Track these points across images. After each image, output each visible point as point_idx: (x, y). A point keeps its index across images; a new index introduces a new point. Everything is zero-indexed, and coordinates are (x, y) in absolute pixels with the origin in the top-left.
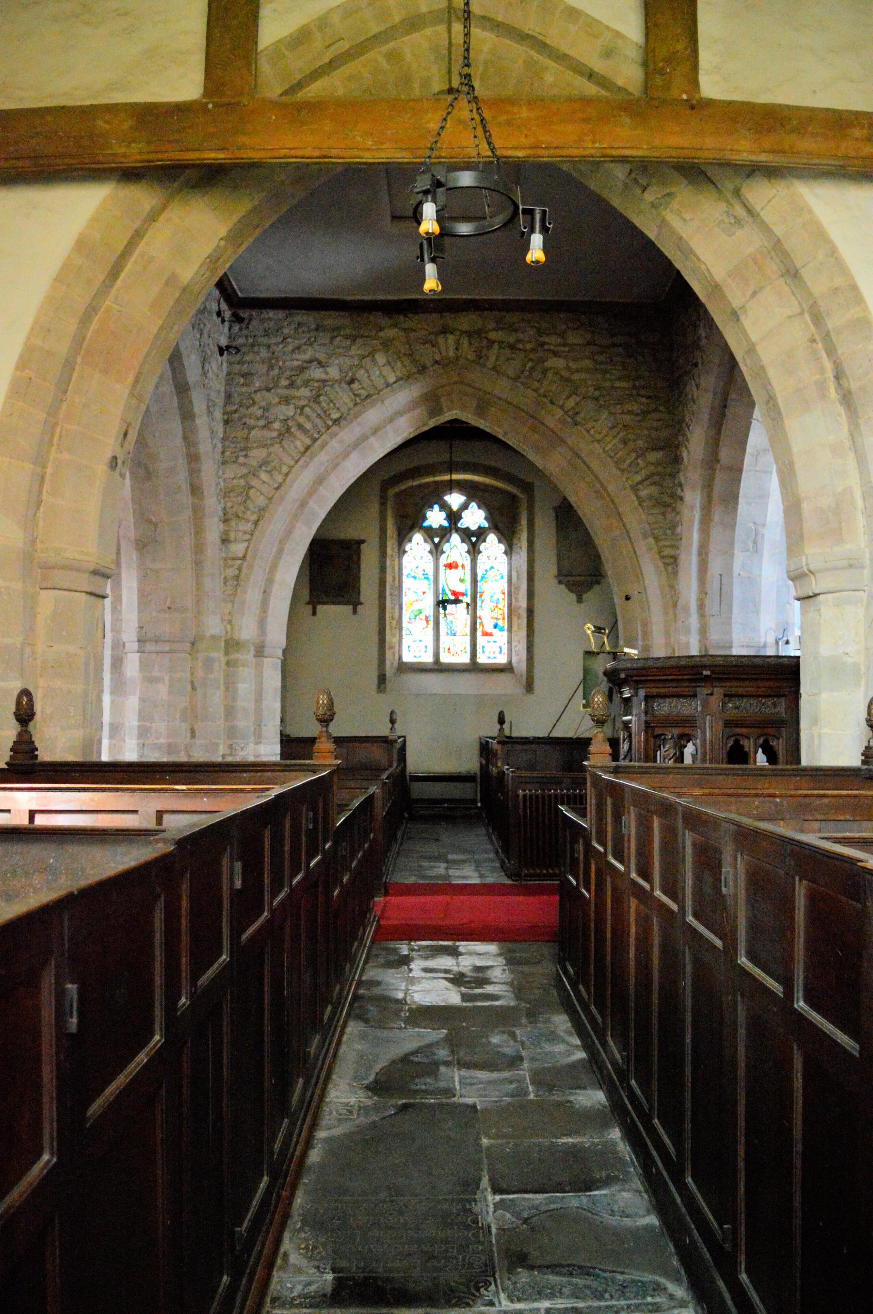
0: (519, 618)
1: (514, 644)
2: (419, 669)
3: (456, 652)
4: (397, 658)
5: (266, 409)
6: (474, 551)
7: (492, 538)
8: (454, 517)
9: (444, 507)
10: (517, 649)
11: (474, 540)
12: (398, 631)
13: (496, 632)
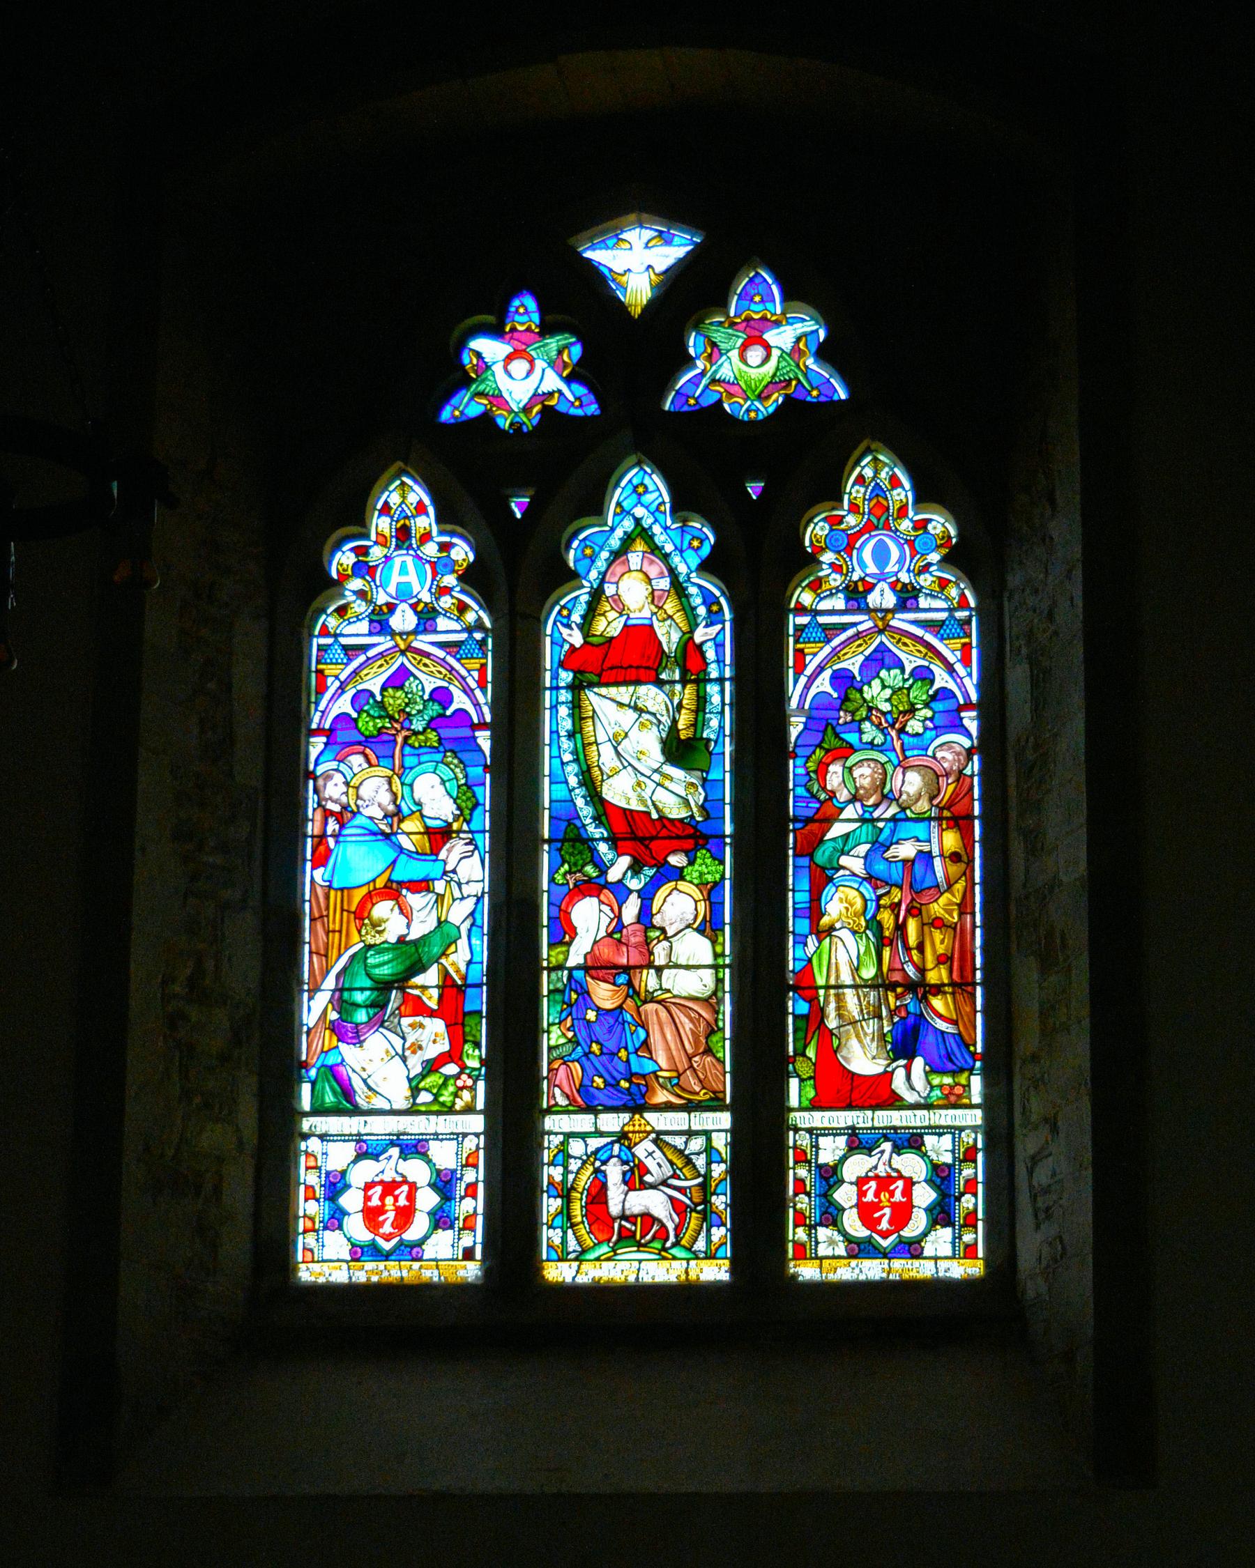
0: (1047, 964)
1: (1027, 1145)
2: (388, 1320)
3: (638, 1215)
4: (236, 1247)
5: (328, 813)
6: (759, 570)
7: (878, 475)
8: (629, 353)
9: (580, 303)
10: (1042, 1176)
11: (756, 500)
12: (248, 1086)
13: (912, 1079)
